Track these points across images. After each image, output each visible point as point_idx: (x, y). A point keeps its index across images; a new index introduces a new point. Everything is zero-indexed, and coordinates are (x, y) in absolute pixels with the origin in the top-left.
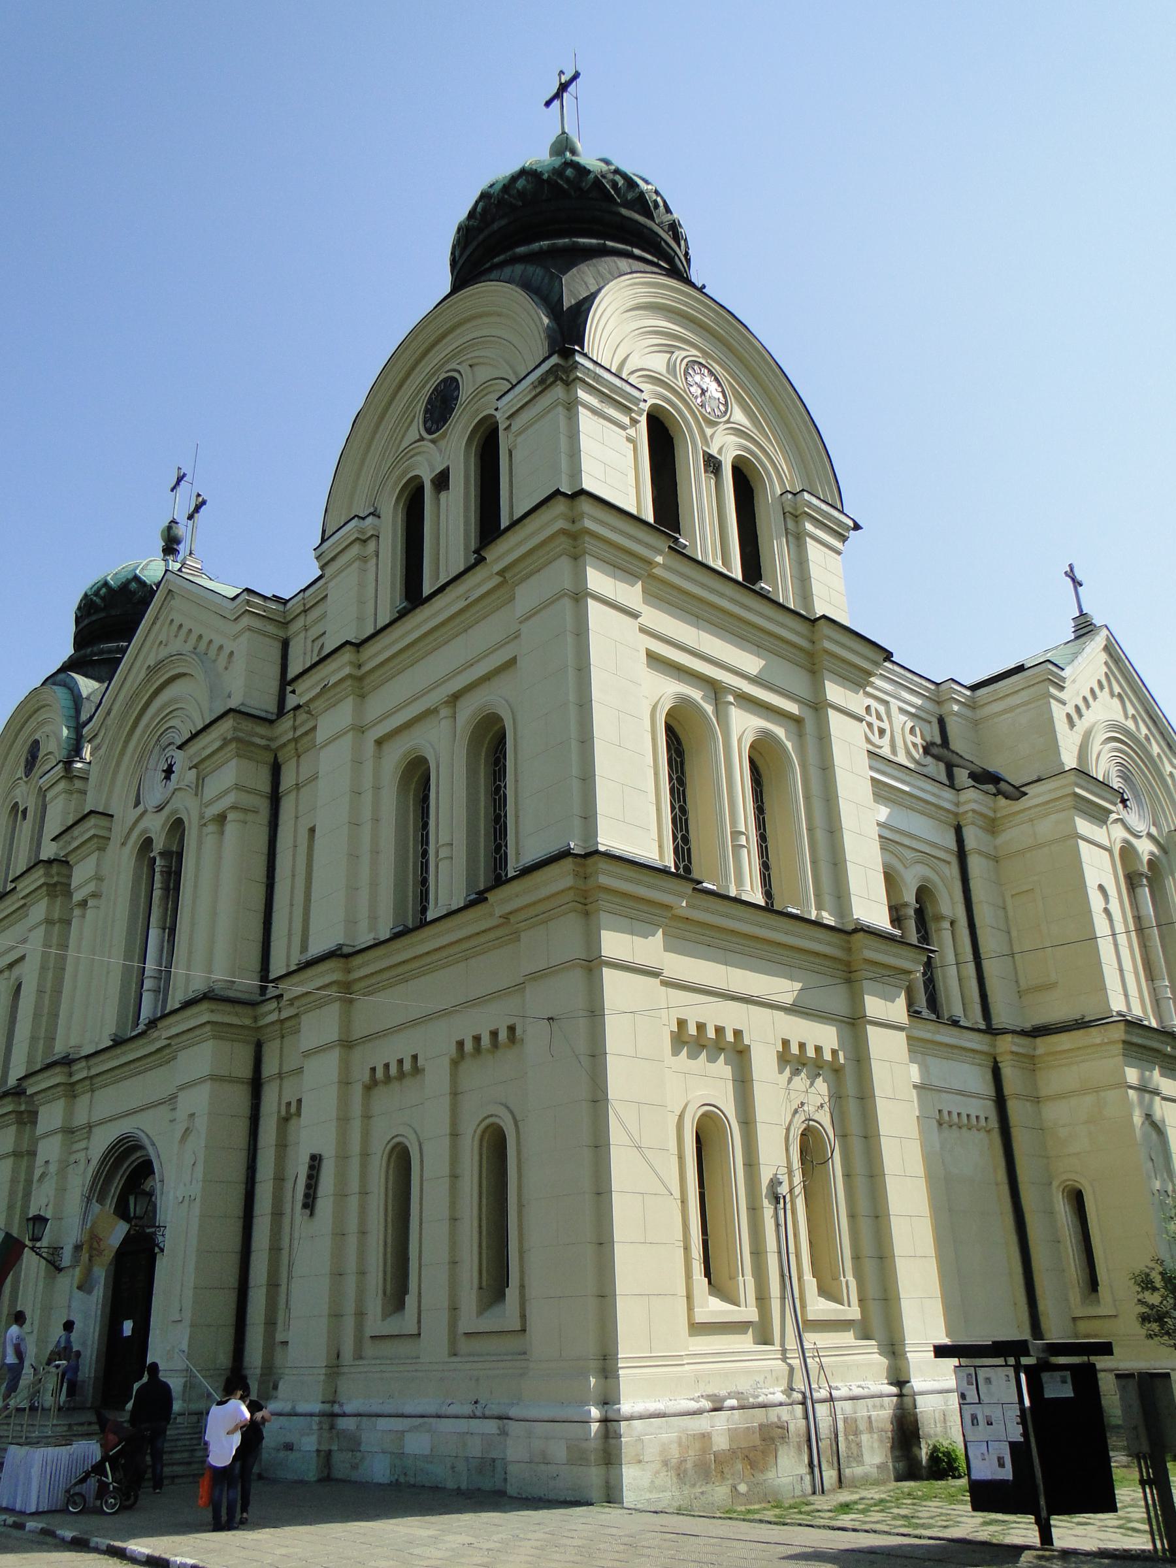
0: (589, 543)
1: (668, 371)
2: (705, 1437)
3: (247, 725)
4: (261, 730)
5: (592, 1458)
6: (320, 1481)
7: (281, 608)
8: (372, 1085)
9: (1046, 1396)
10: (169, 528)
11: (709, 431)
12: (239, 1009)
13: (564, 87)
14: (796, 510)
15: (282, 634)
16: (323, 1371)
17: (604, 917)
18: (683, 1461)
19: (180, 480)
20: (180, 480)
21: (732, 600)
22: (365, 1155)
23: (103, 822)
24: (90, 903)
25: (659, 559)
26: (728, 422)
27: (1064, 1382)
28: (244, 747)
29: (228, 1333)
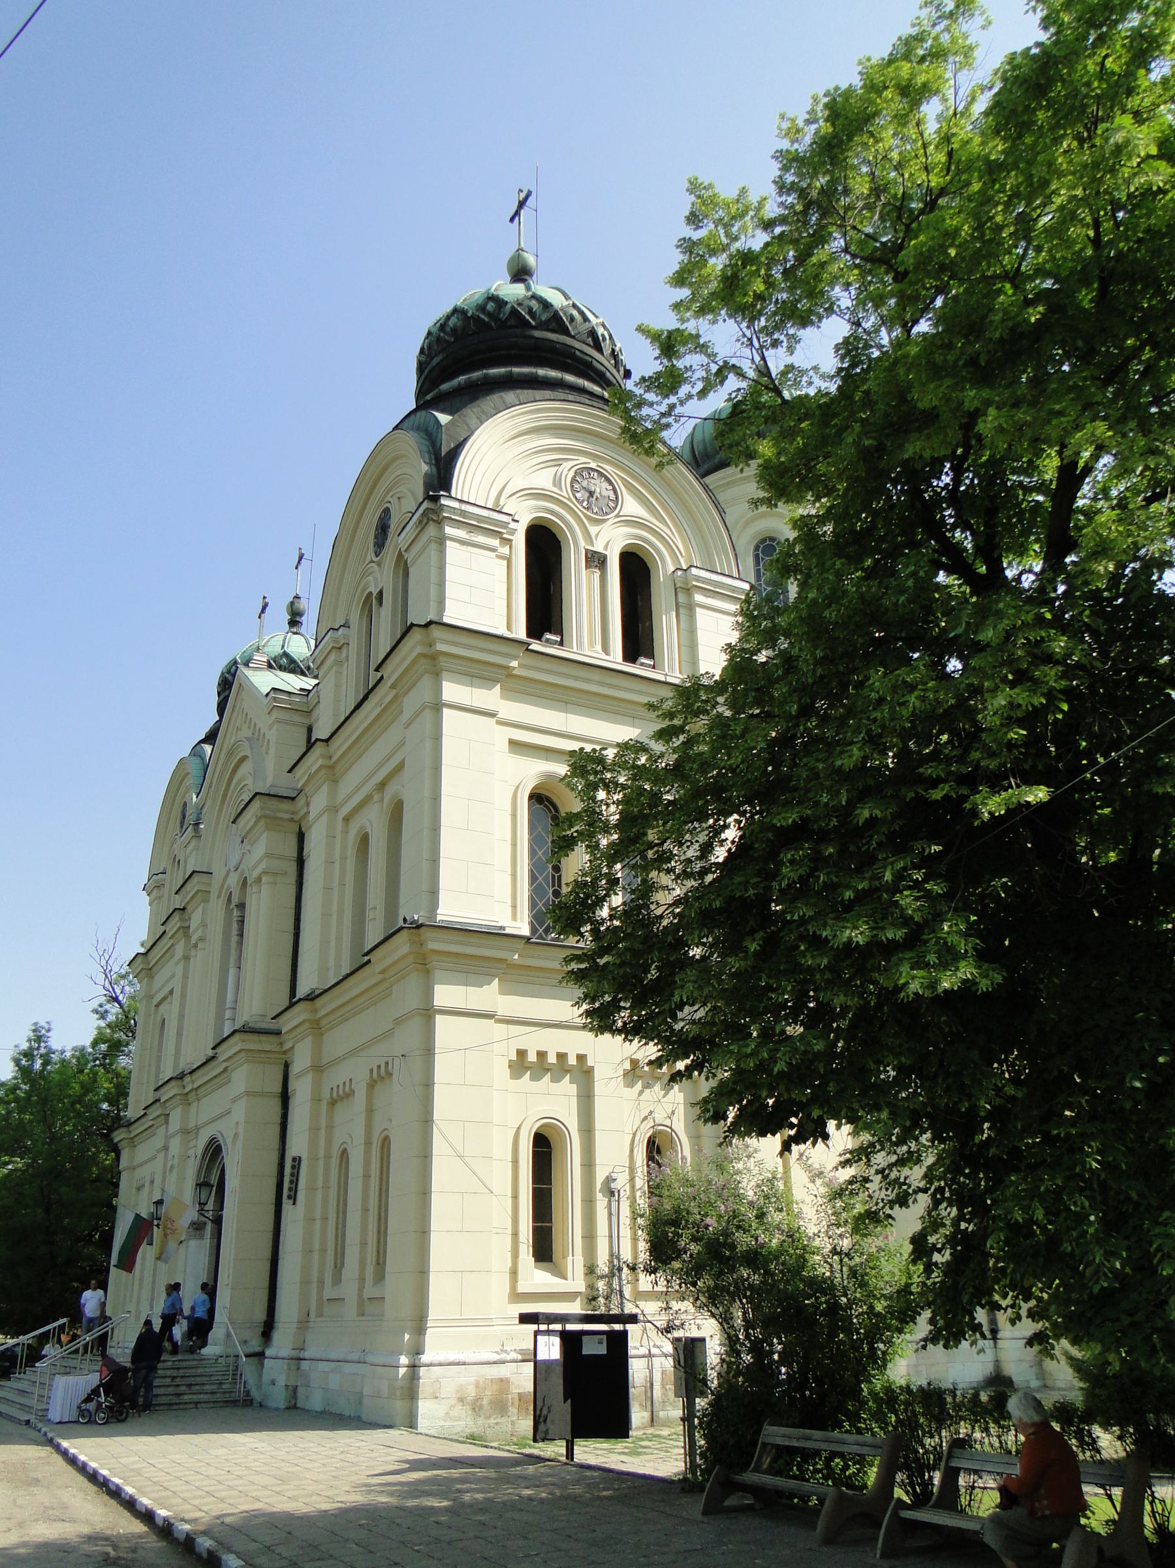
0: (443, 662)
1: (554, 485)
2: (503, 1382)
3: (273, 804)
4: (286, 805)
5: (398, 1393)
6: (288, 1408)
7: (304, 699)
8: (333, 1103)
9: (584, 1353)
10: (292, 603)
11: (593, 530)
12: (263, 1038)
13: (522, 204)
14: (687, 584)
15: (306, 721)
16: (295, 1325)
17: (438, 974)
18: (478, 1399)
19: (301, 558)
20: (301, 558)
21: (600, 683)
22: (328, 1157)
23: (204, 878)
24: (199, 946)
25: (514, 664)
26: (618, 516)
27: (600, 1343)
28: (272, 822)
29: (264, 1295)
